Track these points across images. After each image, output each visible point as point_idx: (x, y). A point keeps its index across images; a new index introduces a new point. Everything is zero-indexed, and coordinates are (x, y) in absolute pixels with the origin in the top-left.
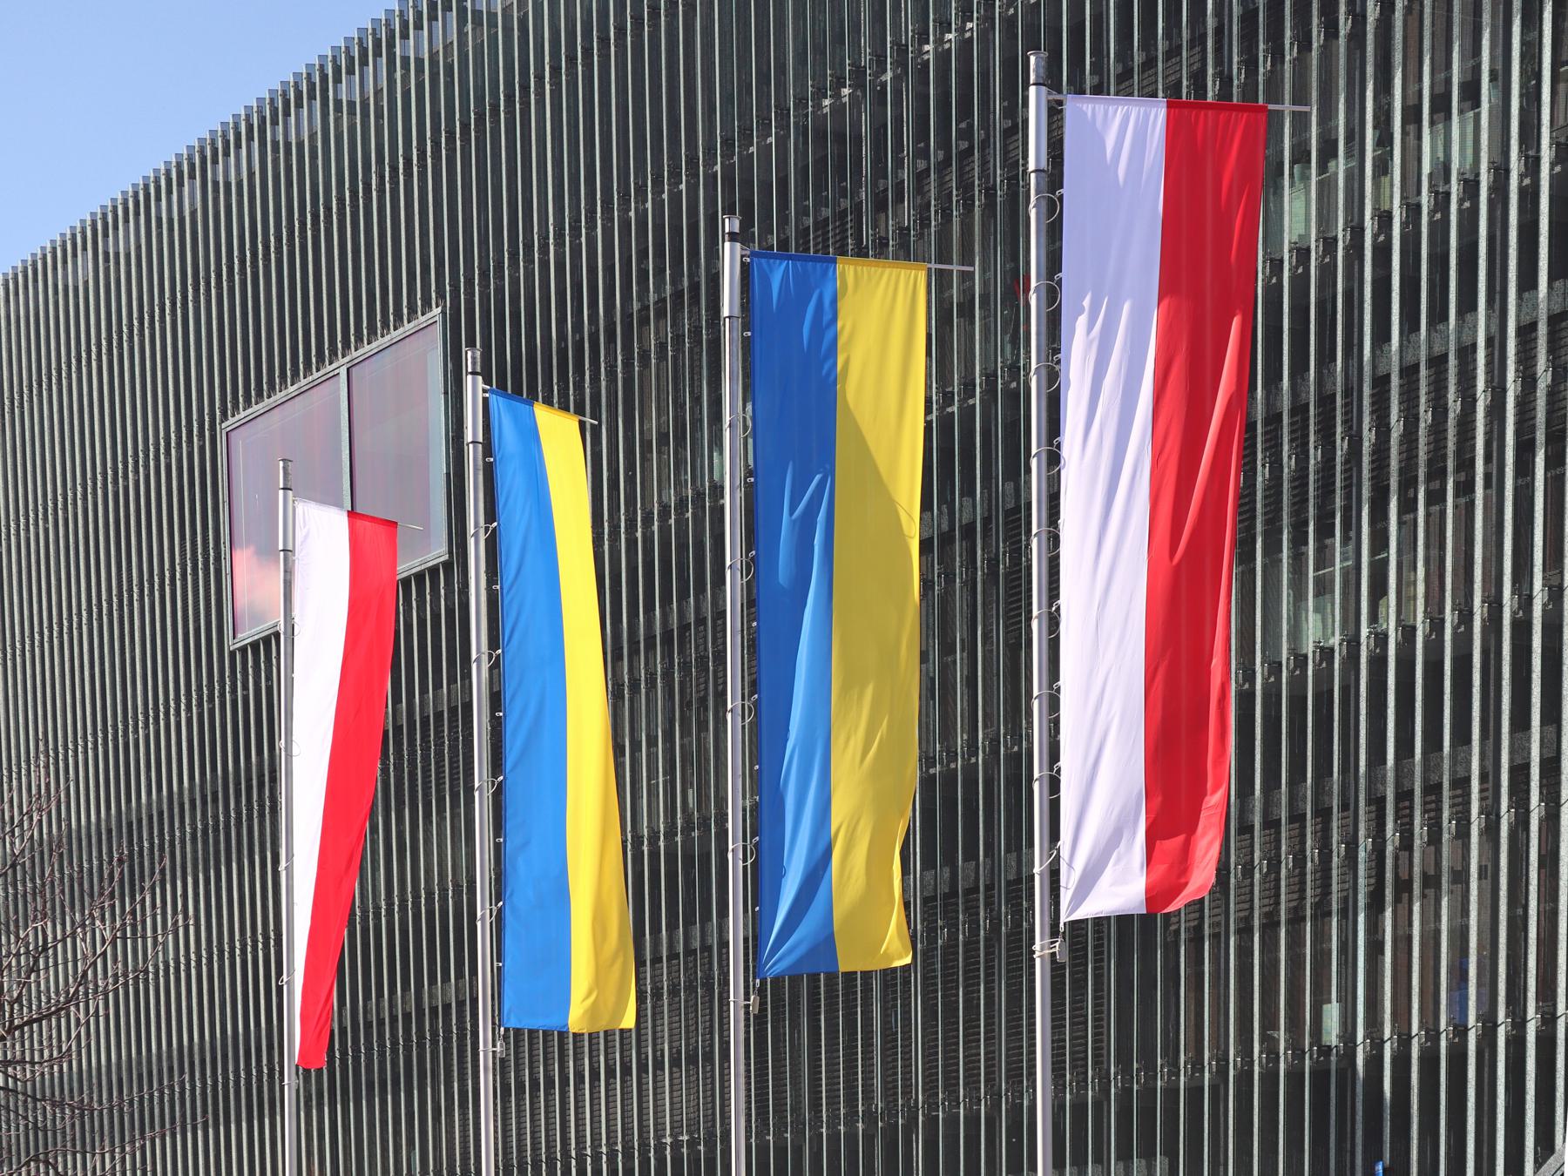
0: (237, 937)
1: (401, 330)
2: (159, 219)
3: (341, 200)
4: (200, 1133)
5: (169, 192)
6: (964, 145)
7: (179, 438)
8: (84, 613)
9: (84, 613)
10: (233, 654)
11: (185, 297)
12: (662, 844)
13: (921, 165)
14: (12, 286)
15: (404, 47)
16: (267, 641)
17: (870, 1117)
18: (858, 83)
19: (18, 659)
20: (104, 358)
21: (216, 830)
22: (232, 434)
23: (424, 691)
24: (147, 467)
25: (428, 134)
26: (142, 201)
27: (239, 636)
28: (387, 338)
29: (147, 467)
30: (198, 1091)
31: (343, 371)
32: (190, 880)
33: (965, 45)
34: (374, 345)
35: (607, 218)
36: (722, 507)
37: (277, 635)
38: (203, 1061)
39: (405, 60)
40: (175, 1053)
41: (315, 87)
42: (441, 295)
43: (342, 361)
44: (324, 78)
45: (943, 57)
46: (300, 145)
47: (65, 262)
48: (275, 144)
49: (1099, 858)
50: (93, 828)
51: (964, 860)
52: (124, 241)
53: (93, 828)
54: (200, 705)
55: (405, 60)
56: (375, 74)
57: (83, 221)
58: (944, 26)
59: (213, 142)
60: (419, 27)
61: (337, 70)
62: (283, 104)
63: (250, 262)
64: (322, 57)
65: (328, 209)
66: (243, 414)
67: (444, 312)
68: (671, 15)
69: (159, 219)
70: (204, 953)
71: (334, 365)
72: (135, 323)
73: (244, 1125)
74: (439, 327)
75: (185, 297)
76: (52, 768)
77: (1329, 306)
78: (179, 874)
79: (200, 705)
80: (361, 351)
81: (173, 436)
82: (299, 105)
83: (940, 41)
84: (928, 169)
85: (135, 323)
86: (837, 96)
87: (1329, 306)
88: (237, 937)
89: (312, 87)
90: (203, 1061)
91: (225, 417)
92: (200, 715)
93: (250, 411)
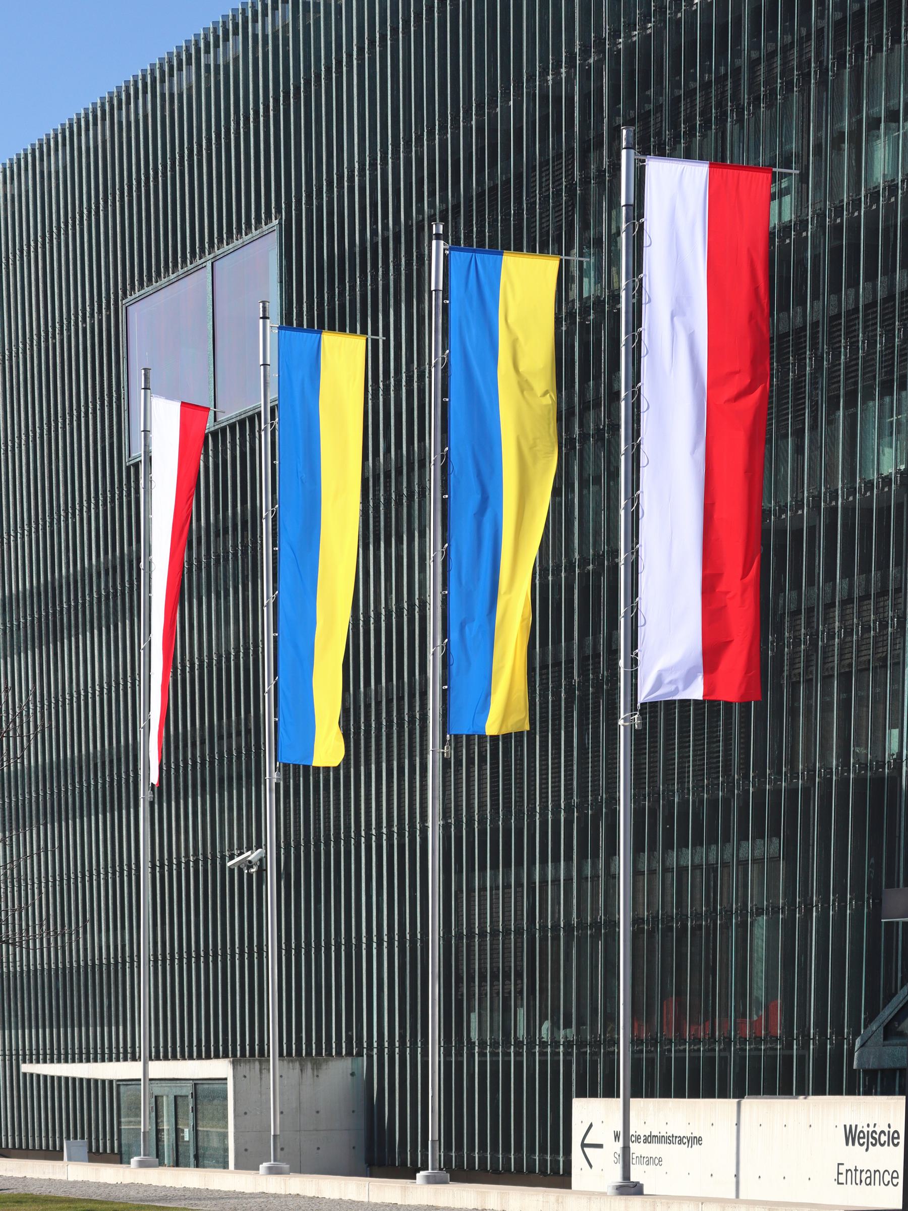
0: (129, 674)
1: (250, 236)
2: (120, 123)
3: (256, 113)
4: (100, 816)
5: (95, 124)
6: (839, 16)
7: (92, 309)
8: (23, 437)
9: (60, 420)
10: (128, 468)
11: (97, 208)
12: (550, 578)
13: (754, 55)
14: (13, 172)
15: (208, 59)
16: (251, 419)
17: (569, 809)
18: (600, 50)
19: (23, 447)
20: (40, 250)
21: (115, 596)
22: (217, 264)
23: (106, 553)
24: (69, 330)
25: (223, 123)
26: (69, 135)
27: (133, 455)
28: (240, 241)
29: (69, 330)
30: (100, 786)
31: (209, 264)
32: (96, 632)
33: (646, 39)
34: (231, 246)
35: (455, 127)
36: (619, 310)
37: (259, 414)
38: (111, 762)
39: (208, 67)
40: (122, 749)
41: (191, 55)
42: (278, 211)
43: (208, 257)
44: (226, 32)
45: (630, 47)
46: (227, 66)
47: (57, 150)
48: (163, 95)
49: (669, 643)
50: (28, 593)
51: (842, 578)
52: (56, 162)
53: (28, 593)
54: (105, 504)
55: (208, 67)
56: (102, 131)
57: (18, 155)
58: (631, 26)
59: (244, 11)
60: (217, 46)
61: (226, 32)
62: (169, 68)
63: (150, 180)
64: (170, 54)
65: (256, 113)
66: (137, 294)
67: (280, 223)
68: (442, 11)
69: (120, 123)
70: (53, 700)
71: (203, 260)
72: (85, 211)
73: (132, 810)
74: (275, 235)
75: (97, 208)
76: (26, 538)
77: (892, 235)
78: (88, 627)
79: (105, 504)
80: (221, 251)
81: (88, 309)
82: (180, 69)
83: (629, 36)
84: (793, 42)
85: (62, 225)
86: (629, 36)
87: (892, 235)
88: (129, 674)
89: (236, 26)
90: (111, 762)
91: (125, 295)
92: (105, 512)
93: (142, 292)
